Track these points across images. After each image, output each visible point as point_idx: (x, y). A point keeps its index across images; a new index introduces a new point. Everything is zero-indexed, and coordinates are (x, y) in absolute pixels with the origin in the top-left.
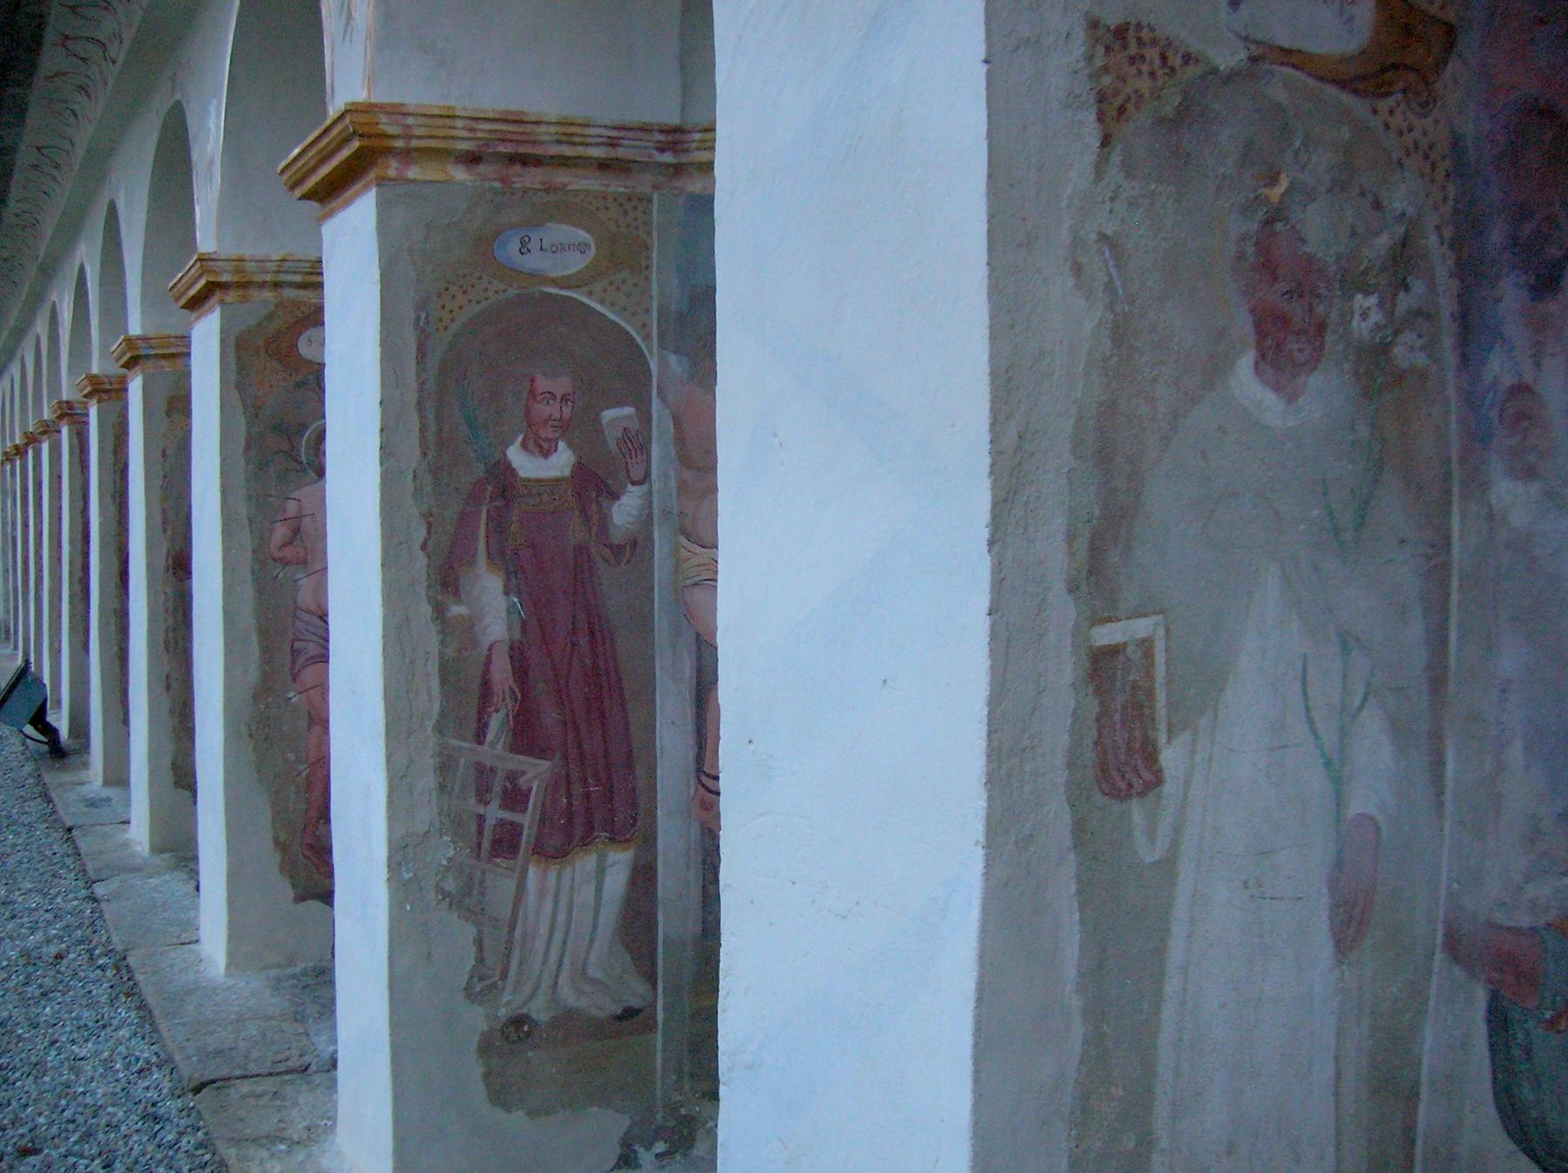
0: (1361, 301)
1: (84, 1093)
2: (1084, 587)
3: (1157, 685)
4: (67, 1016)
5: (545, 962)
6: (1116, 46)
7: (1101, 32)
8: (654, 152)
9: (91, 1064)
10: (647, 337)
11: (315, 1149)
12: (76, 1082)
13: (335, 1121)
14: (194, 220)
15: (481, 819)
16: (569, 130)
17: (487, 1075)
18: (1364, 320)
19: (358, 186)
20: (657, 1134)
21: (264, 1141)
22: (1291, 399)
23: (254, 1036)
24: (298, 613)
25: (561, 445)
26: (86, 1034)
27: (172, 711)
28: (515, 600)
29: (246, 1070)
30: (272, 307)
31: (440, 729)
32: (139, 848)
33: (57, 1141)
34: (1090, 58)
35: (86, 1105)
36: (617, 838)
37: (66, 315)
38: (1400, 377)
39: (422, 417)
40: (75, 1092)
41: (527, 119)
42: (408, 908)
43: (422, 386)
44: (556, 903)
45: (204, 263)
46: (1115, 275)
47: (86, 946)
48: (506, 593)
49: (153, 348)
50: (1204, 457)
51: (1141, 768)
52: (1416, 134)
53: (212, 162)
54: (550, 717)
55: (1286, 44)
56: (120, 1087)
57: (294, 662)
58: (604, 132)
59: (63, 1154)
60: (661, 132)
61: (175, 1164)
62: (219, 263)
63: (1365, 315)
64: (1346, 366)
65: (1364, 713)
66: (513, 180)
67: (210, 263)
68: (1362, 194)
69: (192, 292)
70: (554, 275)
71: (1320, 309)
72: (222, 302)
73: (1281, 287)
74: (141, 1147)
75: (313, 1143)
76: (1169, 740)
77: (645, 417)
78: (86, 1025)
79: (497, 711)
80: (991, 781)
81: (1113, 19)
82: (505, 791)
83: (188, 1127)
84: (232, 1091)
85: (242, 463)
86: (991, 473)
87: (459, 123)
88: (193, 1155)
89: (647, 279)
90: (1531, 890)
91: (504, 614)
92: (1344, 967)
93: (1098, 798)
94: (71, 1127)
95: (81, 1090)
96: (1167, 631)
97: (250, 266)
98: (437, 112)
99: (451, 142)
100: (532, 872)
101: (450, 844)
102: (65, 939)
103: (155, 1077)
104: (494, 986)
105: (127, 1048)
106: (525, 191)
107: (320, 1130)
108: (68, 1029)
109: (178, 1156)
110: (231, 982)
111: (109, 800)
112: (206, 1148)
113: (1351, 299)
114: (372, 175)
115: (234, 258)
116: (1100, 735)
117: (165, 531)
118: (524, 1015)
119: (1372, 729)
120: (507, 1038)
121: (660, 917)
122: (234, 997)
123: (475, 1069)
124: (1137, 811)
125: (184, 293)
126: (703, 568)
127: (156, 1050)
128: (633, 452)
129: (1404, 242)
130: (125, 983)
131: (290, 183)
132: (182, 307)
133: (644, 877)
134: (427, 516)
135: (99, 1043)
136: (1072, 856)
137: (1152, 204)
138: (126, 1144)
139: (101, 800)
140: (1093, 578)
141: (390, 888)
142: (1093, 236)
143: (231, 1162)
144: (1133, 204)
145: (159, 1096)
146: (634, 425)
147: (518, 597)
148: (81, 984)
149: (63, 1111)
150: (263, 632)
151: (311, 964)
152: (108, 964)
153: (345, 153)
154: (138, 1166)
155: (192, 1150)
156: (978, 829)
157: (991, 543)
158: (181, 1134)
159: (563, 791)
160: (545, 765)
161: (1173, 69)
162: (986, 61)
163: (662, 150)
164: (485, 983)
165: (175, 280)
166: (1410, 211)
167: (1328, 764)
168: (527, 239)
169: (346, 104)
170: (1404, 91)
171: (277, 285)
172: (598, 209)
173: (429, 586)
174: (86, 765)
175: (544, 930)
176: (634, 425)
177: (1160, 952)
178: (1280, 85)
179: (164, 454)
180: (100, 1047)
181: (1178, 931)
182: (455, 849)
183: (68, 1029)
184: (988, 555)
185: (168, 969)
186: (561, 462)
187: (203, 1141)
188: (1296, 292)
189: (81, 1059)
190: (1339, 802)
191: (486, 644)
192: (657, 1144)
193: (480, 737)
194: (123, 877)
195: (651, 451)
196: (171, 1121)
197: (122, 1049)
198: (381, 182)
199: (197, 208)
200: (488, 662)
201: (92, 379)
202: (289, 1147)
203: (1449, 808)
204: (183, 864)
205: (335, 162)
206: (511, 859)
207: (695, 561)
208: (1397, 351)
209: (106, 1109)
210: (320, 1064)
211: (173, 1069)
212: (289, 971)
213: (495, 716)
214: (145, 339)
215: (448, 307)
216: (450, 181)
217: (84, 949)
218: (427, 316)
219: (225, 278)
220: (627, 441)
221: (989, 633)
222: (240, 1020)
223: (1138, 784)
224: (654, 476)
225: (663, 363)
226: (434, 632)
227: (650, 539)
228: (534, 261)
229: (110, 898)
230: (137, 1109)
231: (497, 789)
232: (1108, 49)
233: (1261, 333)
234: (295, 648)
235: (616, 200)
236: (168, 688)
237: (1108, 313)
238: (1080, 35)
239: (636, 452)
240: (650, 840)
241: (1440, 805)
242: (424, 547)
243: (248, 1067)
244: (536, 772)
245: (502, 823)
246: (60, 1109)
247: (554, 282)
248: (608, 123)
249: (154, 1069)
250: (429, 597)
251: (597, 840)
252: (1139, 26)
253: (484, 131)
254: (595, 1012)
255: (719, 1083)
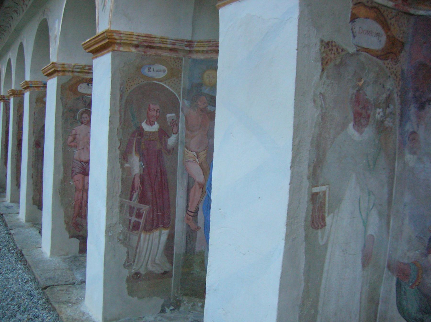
0: (379, 110)
1: (10, 288)
2: (311, 179)
3: (326, 202)
4: (4, 266)
5: (144, 259)
6: (326, 47)
7: (323, 43)
8: (184, 47)
9: (12, 280)
10: (179, 95)
11: (79, 305)
12: (8, 284)
13: (84, 298)
14: (49, 52)
15: (130, 221)
16: (163, 40)
17: (128, 288)
18: (379, 115)
19: (106, 51)
20: (171, 305)
21: (65, 303)
22: (361, 133)
23: (59, 274)
24: (74, 160)
25: (156, 123)
26: (10, 271)
27: (33, 183)
28: (142, 163)
29: (58, 283)
30: (71, 78)
31: (120, 196)
32: (22, 221)
33: (4, 300)
34: (320, 50)
35: (11, 291)
36: (165, 227)
37: (3, 72)
38: (386, 129)
39: (120, 114)
40: (8, 287)
41: (152, 37)
42: (110, 243)
43: (121, 106)
44: (148, 243)
45: (54, 65)
46: (323, 103)
47: (7, 247)
48: (140, 161)
49: (33, 84)
50: (340, 148)
51: (321, 221)
52: (393, 70)
53: (56, 37)
54: (149, 194)
55: (365, 47)
56: (20, 286)
57: (72, 173)
58: (172, 41)
59: (7, 304)
60: (186, 42)
61: (37, 308)
62: (58, 65)
63: (379, 114)
64: (374, 126)
65: (372, 210)
66: (147, 52)
67: (55, 65)
68: (380, 84)
69: (49, 72)
70: (156, 78)
71: (369, 112)
72: (58, 75)
73: (360, 106)
74: (28, 303)
75: (78, 304)
76: (328, 216)
77: (178, 116)
78: (10, 269)
79: (136, 192)
80: (287, 225)
81: (326, 41)
82: (137, 213)
83: (40, 298)
84: (55, 289)
85: (61, 119)
86: (292, 150)
87: (134, 37)
88: (42, 306)
89: (180, 80)
90: (408, 254)
91: (139, 167)
92: (364, 271)
93: (311, 228)
94: (8, 297)
95: (10, 287)
96: (329, 189)
97: (66, 66)
98: (129, 33)
99: (132, 41)
100: (143, 235)
101: (122, 227)
102: (1, 245)
103: (30, 284)
104: (131, 264)
105: (22, 276)
106: (150, 55)
107: (80, 300)
108: (4, 270)
109: (38, 306)
110: (51, 259)
111: (12, 206)
112: (46, 304)
113: (376, 109)
114: (110, 49)
115: (62, 64)
116: (312, 214)
117: (34, 135)
118: (138, 272)
119: (374, 214)
120: (134, 278)
121: (175, 248)
122: (53, 263)
123: (125, 285)
124: (319, 232)
125: (47, 71)
126: (191, 157)
127: (30, 276)
128: (174, 126)
129: (389, 96)
130: (19, 258)
131: (85, 48)
132: (45, 75)
133: (171, 237)
134: (120, 140)
135: (14, 274)
136: (304, 243)
137: (332, 86)
138: (24, 302)
139: (10, 206)
140: (313, 176)
141: (106, 238)
142: (318, 93)
143: (57, 308)
144: (328, 86)
145: (31, 289)
146: (175, 119)
147: (143, 162)
148: (7, 257)
149: (5, 292)
150: (64, 165)
151: (73, 255)
152: (14, 252)
153: (103, 42)
154: (27, 308)
155: (42, 304)
156: (284, 236)
157: (291, 167)
158: (38, 300)
159: (152, 214)
160: (147, 207)
161: (339, 52)
162: (297, 50)
163: (186, 46)
164: (129, 263)
165: (44, 68)
166: (391, 88)
167: (364, 222)
168: (150, 68)
169: (105, 30)
170: (392, 59)
171: (73, 72)
172: (169, 61)
173: (120, 159)
174: (5, 197)
175: (145, 250)
176: (175, 119)
177: (322, 267)
178: (363, 56)
179: (34, 114)
180: (14, 275)
181: (327, 261)
182: (123, 228)
183: (4, 270)
184: (290, 170)
185: (33, 255)
186: (155, 127)
187: (45, 302)
188: (364, 108)
189: (9, 278)
190: (365, 232)
191: (134, 174)
192: (171, 307)
193: (131, 199)
194: (19, 228)
195: (179, 125)
196: (35, 296)
197: (20, 276)
198: (113, 51)
199: (51, 49)
200: (134, 179)
201: (13, 91)
202: (72, 304)
203: (390, 234)
204: (34, 226)
205: (100, 44)
206: (137, 231)
207: (189, 155)
208: (386, 122)
209: (17, 292)
210: (78, 282)
211: (35, 282)
212: (67, 257)
213: (135, 193)
214: (31, 82)
215: (128, 85)
216: (131, 52)
217: (7, 248)
218: (123, 87)
219: (59, 69)
220: (173, 123)
221: (289, 189)
222: (55, 269)
223: (320, 226)
224: (179, 132)
225: (183, 103)
226: (121, 171)
227: (177, 149)
228: (151, 74)
229: (16, 234)
230: (26, 293)
231: (135, 213)
232: (325, 47)
233: (355, 118)
234: (73, 170)
235: (173, 59)
236: (32, 177)
237: (321, 112)
238: (319, 44)
239: (175, 126)
240: (173, 227)
241: (388, 233)
242: (119, 148)
243: (59, 283)
244: (145, 208)
245: (135, 221)
246: (4, 292)
247: (156, 80)
248: (174, 39)
249: (30, 282)
250: (119, 162)
251: (160, 227)
252: (332, 42)
253: (141, 39)
254: (156, 272)
255: (205, 294)
